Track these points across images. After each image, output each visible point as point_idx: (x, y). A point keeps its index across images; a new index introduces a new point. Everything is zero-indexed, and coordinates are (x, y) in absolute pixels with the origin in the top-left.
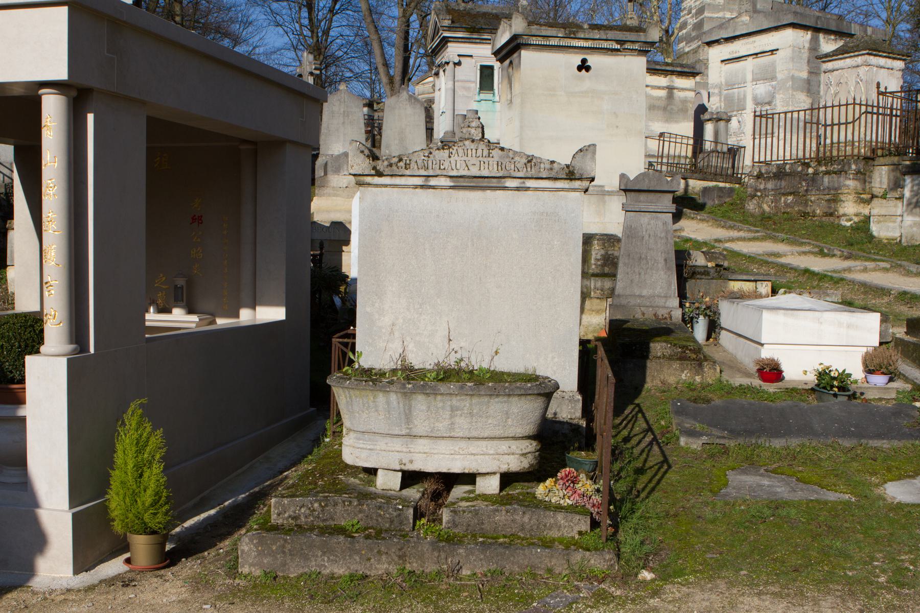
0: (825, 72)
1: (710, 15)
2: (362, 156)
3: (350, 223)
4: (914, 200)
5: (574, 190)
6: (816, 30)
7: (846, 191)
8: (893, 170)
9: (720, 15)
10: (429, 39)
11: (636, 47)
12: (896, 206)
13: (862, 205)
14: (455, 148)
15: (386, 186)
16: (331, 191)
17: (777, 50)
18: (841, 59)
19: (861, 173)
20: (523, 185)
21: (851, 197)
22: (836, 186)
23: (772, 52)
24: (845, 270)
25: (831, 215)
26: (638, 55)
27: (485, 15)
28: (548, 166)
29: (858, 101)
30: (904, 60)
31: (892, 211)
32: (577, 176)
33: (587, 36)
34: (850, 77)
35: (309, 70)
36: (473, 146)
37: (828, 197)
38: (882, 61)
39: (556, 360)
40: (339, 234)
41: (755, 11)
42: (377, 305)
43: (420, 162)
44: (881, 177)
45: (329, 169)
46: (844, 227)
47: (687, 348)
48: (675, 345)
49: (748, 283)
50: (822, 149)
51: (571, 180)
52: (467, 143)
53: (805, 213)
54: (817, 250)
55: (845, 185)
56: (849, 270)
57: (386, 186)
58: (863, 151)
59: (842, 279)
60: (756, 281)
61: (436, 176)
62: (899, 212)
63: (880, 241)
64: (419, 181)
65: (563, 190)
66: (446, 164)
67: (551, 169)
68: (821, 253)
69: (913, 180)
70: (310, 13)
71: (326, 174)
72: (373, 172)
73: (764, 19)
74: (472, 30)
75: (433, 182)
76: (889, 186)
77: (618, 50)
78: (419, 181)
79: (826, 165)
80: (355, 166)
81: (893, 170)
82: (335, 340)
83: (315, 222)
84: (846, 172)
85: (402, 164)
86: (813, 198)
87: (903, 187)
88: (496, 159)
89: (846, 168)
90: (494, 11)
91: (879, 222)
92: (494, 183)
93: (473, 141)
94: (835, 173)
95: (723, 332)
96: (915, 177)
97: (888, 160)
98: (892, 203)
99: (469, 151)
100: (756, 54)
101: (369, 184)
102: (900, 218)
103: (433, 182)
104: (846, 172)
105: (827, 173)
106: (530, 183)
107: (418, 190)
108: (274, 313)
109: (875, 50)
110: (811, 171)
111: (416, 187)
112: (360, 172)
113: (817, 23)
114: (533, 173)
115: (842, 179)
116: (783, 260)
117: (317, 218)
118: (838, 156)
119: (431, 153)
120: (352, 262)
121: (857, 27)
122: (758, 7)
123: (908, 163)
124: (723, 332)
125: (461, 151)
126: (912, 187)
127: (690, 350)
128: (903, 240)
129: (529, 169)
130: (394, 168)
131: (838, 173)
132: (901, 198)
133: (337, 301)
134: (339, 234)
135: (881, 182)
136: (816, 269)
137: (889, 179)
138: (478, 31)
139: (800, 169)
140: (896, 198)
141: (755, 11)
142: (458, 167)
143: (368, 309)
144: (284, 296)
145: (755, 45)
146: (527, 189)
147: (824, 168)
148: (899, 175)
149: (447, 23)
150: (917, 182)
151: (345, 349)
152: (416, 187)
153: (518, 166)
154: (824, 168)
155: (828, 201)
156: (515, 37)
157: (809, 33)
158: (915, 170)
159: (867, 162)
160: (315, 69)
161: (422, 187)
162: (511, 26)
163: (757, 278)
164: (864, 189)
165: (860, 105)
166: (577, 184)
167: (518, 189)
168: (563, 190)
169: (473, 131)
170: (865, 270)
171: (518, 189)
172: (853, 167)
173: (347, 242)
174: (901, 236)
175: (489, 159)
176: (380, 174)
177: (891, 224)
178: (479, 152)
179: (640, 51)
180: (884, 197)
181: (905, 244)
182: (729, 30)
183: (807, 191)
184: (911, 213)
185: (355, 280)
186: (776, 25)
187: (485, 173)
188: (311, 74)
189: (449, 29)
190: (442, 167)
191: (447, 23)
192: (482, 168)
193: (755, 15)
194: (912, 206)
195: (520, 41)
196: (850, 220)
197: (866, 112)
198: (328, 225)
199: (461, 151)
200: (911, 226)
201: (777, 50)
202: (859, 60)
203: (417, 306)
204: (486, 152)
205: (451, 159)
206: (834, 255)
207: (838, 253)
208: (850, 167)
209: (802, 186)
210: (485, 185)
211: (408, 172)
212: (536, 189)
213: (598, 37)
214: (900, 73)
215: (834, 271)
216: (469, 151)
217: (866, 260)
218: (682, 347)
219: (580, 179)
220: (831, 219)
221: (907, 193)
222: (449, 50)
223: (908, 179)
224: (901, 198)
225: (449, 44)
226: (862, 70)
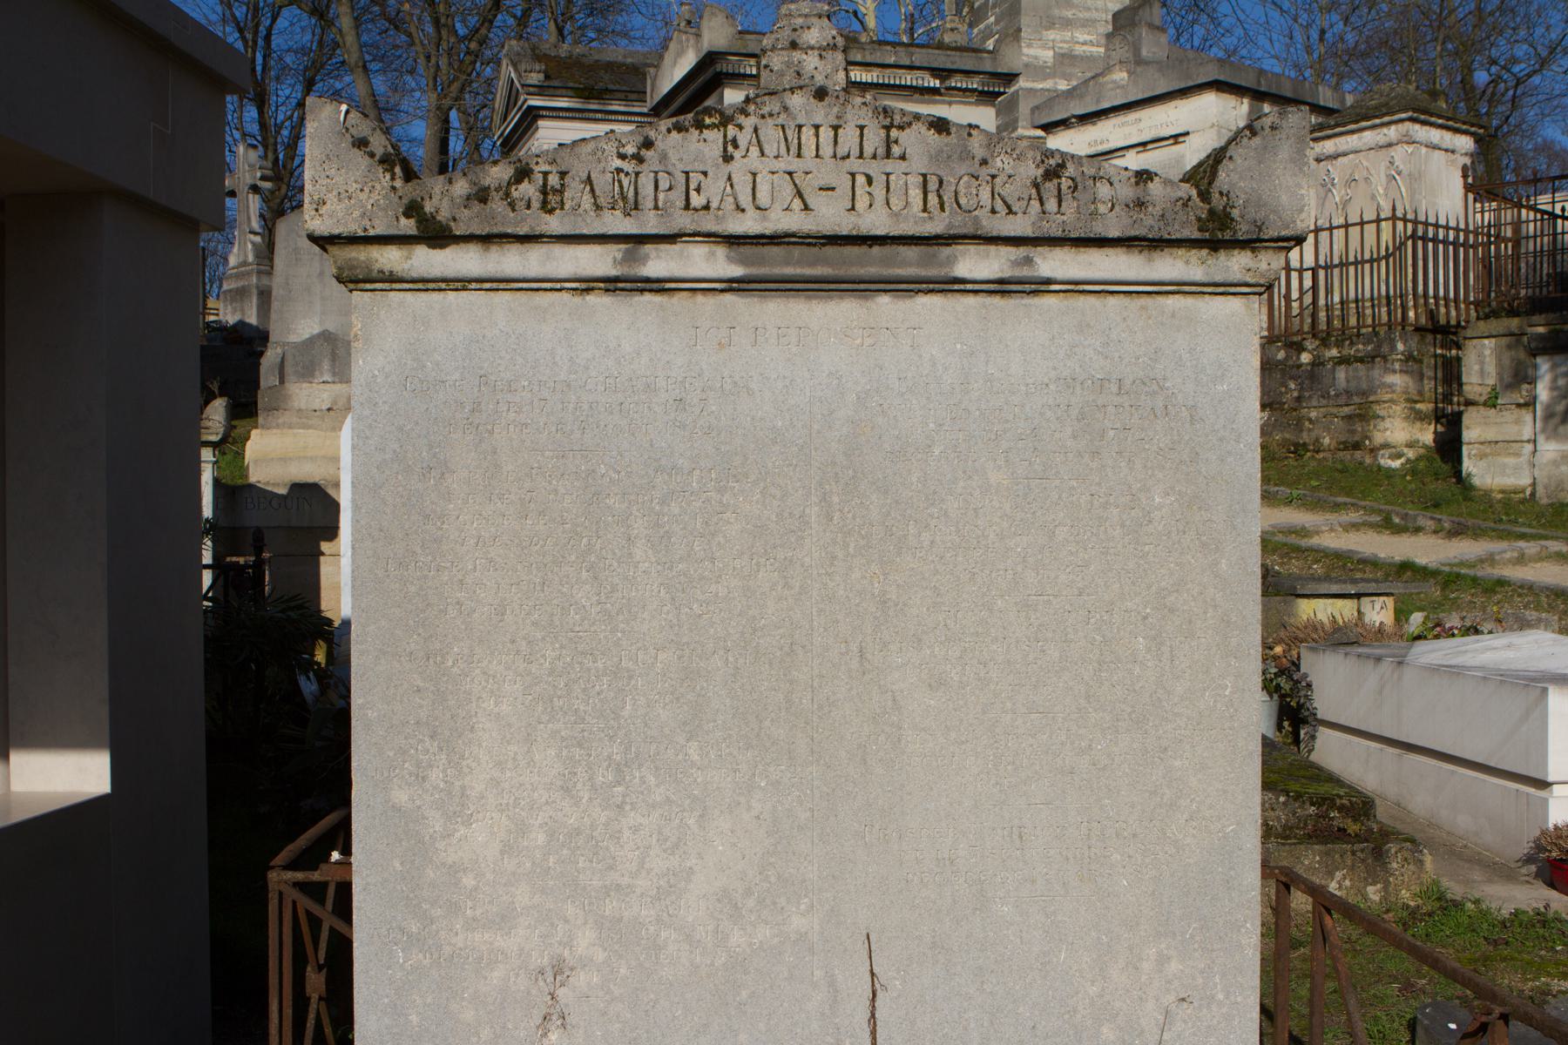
0: (1318, 160)
1: (1029, 85)
2: (360, 160)
3: (337, 485)
4: (1560, 408)
5: (1223, 288)
6: (1258, 96)
7: (1387, 397)
8: (1509, 347)
9: (1048, 84)
10: (497, 119)
11: (974, 84)
12: (1518, 422)
13: (1418, 424)
14: (749, 123)
15: (461, 284)
16: (295, 420)
17: (1187, 134)
18: (1353, 132)
19: (1415, 360)
20: (1025, 272)
21: (1398, 409)
22: (1364, 386)
23: (1176, 138)
24: (1482, 561)
25: (1357, 446)
26: (978, 103)
27: (610, 66)
28: (1126, 192)
29: (1399, 214)
30: (1472, 134)
31: (1510, 431)
32: (1243, 231)
33: (869, 59)
34: (1377, 168)
35: (249, 181)
36: (821, 113)
37: (1346, 410)
38: (1435, 135)
39: (1174, 966)
40: (312, 511)
41: (1139, 61)
42: (435, 776)
43: (603, 182)
44: (1482, 363)
45: (289, 369)
46: (1389, 469)
47: (1333, 806)
48: (1298, 796)
49: (1340, 602)
50: (1322, 315)
51: (1214, 245)
52: (796, 100)
53: (1296, 445)
54: (1376, 518)
55: (1384, 385)
56: (1490, 559)
57: (461, 284)
58: (1411, 314)
59: (1501, 582)
60: (1358, 596)
61: (671, 238)
62: (1527, 433)
63: (1487, 493)
64: (597, 261)
65: (1180, 288)
66: (714, 189)
67: (1140, 204)
68: (1387, 526)
69: (1554, 367)
70: (261, 113)
71: (282, 381)
72: (408, 226)
73: (1157, 75)
74: (587, 93)
75: (658, 263)
76: (1500, 375)
77: (934, 91)
78: (597, 261)
79: (1339, 345)
80: (333, 205)
81: (1509, 347)
82: (279, 878)
83: (251, 486)
84: (1385, 358)
85: (527, 189)
86: (1313, 414)
87: (1533, 382)
88: (918, 163)
89: (1385, 349)
90: (629, 60)
91: (1482, 456)
92: (909, 262)
93: (821, 94)
94: (1361, 360)
95: (1324, 734)
96: (1558, 358)
97: (1495, 325)
98: (1509, 415)
99: (808, 133)
100: (1144, 144)
101: (392, 280)
102: (1530, 447)
103: (658, 263)
104: (1385, 358)
105: (1343, 361)
106: (1054, 264)
107: (596, 300)
108: (72, 775)
109: (1424, 112)
110: (1305, 358)
111: (587, 285)
112: (353, 227)
113: (1259, 83)
114: (1068, 218)
115: (1376, 373)
116: (1315, 541)
117: (256, 476)
118: (1359, 327)
119: (648, 144)
120: (343, 581)
121: (1329, 93)
122: (1144, 53)
123: (1541, 330)
124: (1324, 734)
125: (770, 133)
126: (1554, 380)
127: (1341, 809)
128: (1540, 491)
129: (1051, 205)
130: (497, 205)
131: (1368, 359)
132: (1530, 403)
133: (309, 687)
134: (312, 511)
135: (1482, 372)
136: (1421, 560)
137: (1499, 364)
138: (601, 94)
139: (1281, 355)
140: (1519, 405)
141: (1139, 61)
142: (763, 197)
143: (401, 796)
144: (104, 712)
145: (1141, 126)
146: (1041, 286)
147: (1334, 352)
148: (1522, 355)
149: (535, 78)
150: (1563, 369)
151: (316, 909)
152: (587, 285)
153: (1008, 191)
154: (1334, 352)
155: (1349, 418)
156: (709, 60)
157: (1246, 101)
158: (1556, 346)
159: (1423, 338)
160: (263, 178)
161: (611, 284)
162: (698, 35)
163: (1362, 587)
164: (1420, 393)
165: (1405, 220)
166: (1236, 264)
167: (1002, 287)
168: (1180, 288)
169: (811, 62)
170: (1521, 560)
171: (1002, 287)
172: (1400, 346)
173: (332, 532)
174: (1534, 484)
175: (890, 165)
176: (436, 235)
177: (1511, 461)
178: (849, 137)
179: (982, 93)
180: (1491, 403)
181: (1545, 501)
182: (1088, 99)
183: (1299, 399)
184: (1553, 435)
185: (346, 624)
186: (1183, 85)
187: (876, 222)
188: (255, 189)
189: (541, 90)
190: (696, 200)
191: (535, 78)
192: (862, 203)
193: (1139, 69)
194: (1556, 420)
195: (722, 67)
196: (1399, 456)
197: (1414, 236)
198: (283, 491)
199: (770, 133)
200: (1555, 463)
201: (1187, 134)
202: (1392, 132)
203: (604, 776)
204: (874, 139)
205: (738, 168)
206: (1418, 530)
207: (1430, 524)
208: (1393, 348)
209: (1289, 390)
210: (872, 271)
211: (554, 224)
212: (1076, 287)
213: (892, 60)
214: (1468, 161)
215: (1462, 564)
216: (808, 133)
217: (1500, 538)
218: (1320, 801)
219: (1251, 244)
220: (1358, 454)
221: (1543, 392)
222: (540, 133)
223: (1544, 365)
224: (1530, 403)
225: (541, 123)
226: (1399, 153)
